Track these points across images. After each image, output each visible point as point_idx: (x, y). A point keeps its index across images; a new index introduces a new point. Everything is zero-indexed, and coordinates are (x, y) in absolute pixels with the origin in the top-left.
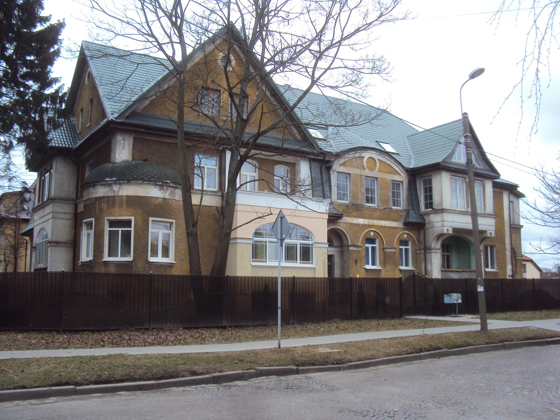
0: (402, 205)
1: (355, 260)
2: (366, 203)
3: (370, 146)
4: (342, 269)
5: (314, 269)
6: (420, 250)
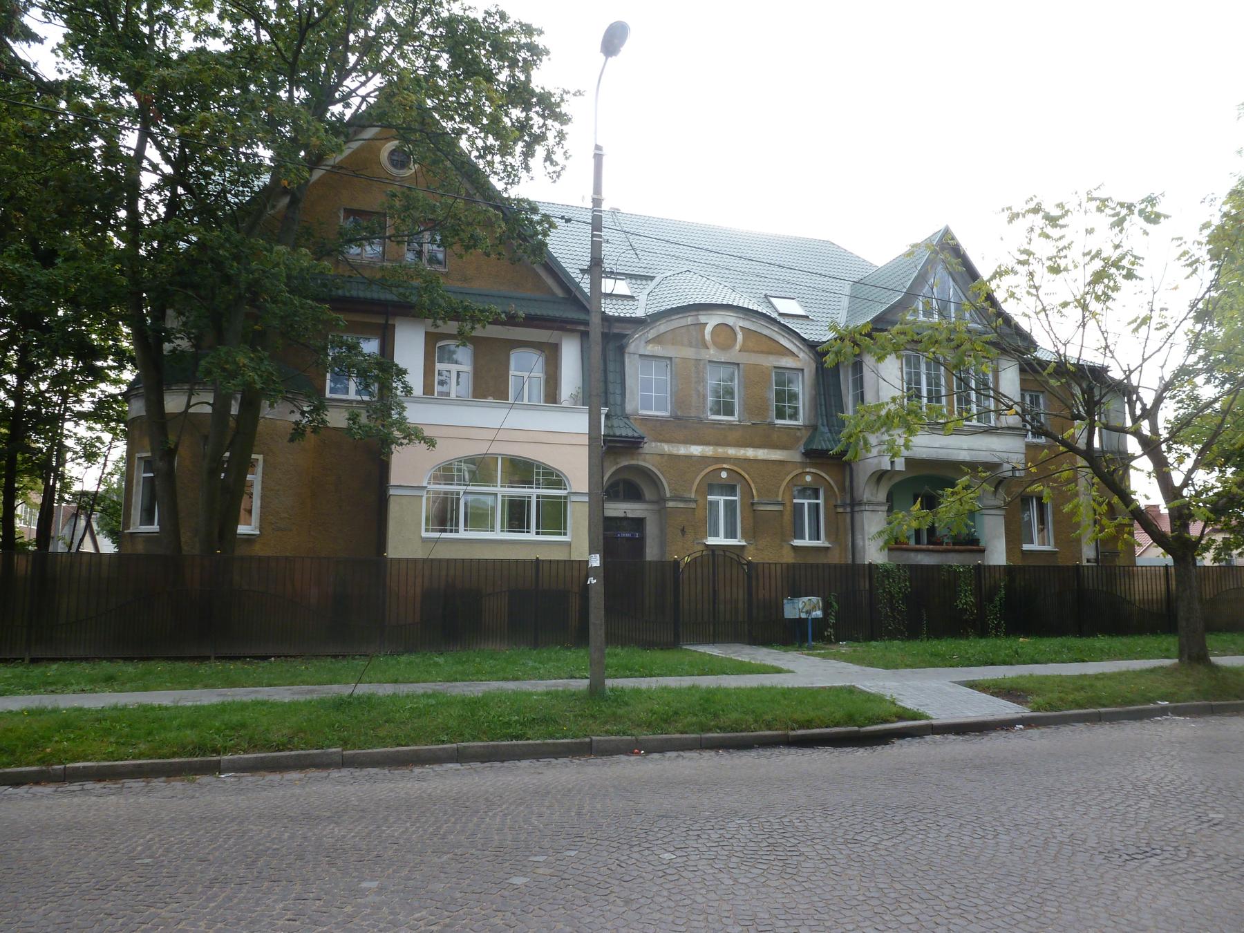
0: (736, 413)
1: (681, 528)
2: (777, 418)
3: (725, 303)
4: (663, 544)
5: (568, 544)
6: (844, 506)
